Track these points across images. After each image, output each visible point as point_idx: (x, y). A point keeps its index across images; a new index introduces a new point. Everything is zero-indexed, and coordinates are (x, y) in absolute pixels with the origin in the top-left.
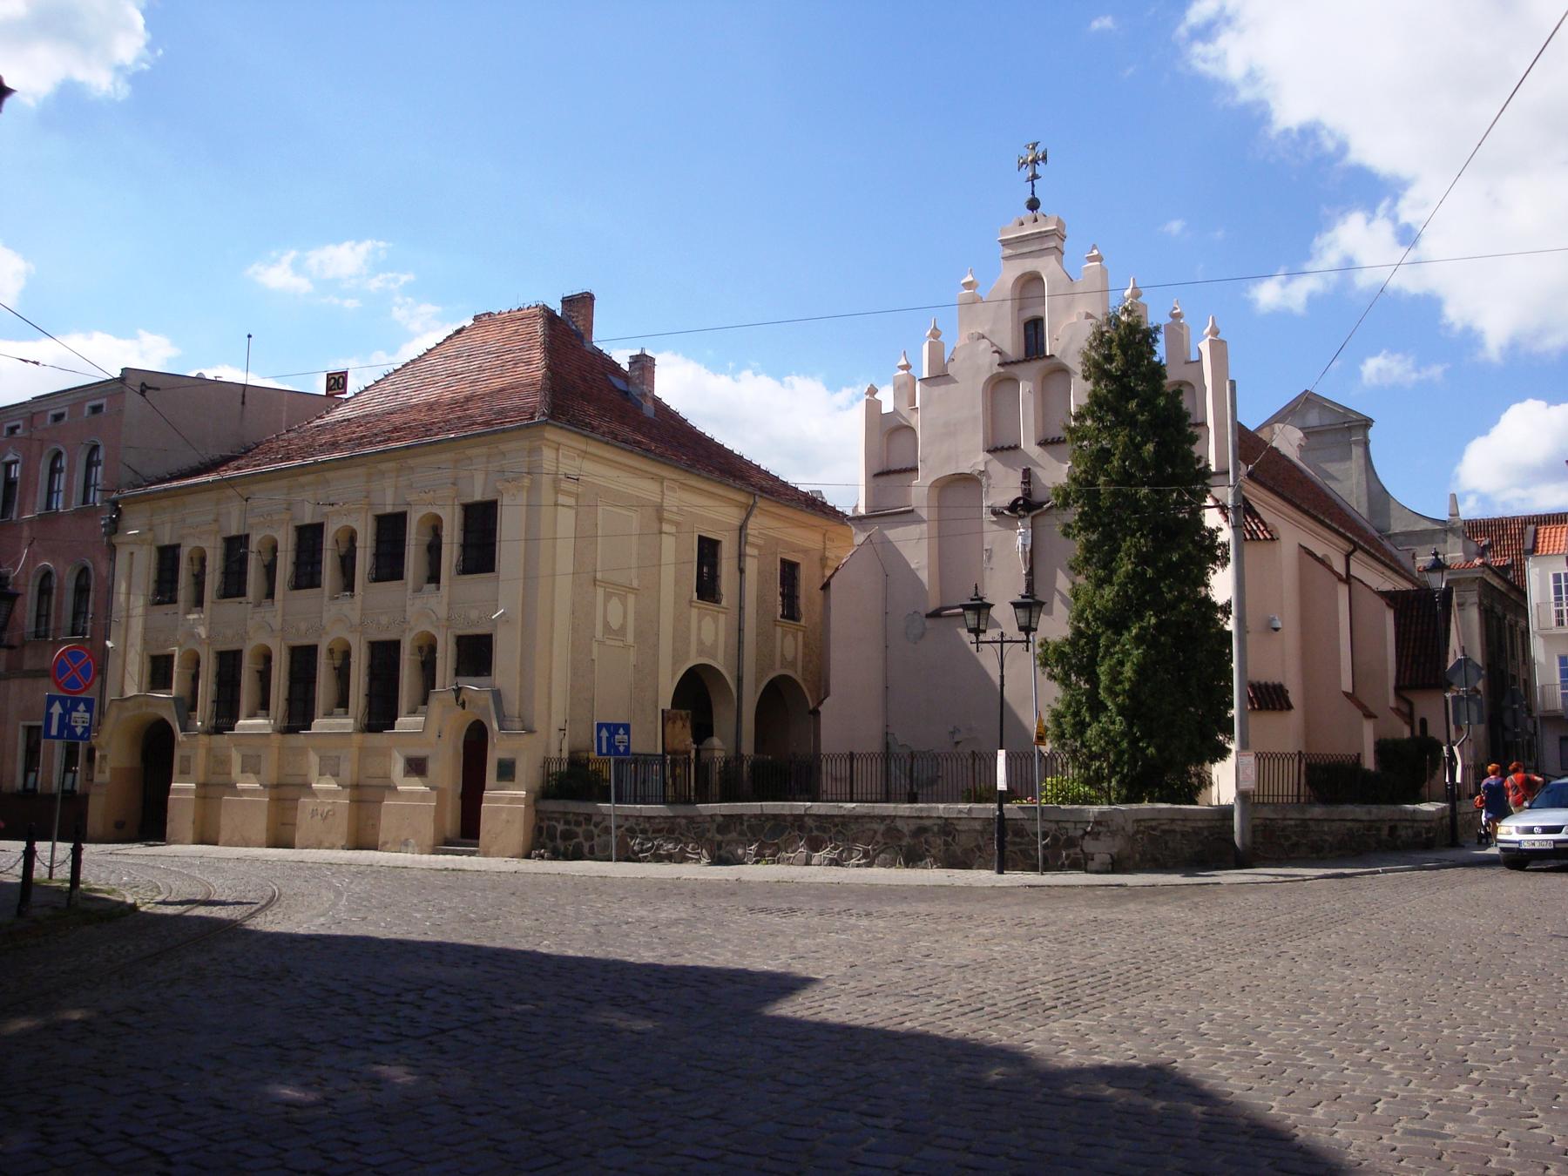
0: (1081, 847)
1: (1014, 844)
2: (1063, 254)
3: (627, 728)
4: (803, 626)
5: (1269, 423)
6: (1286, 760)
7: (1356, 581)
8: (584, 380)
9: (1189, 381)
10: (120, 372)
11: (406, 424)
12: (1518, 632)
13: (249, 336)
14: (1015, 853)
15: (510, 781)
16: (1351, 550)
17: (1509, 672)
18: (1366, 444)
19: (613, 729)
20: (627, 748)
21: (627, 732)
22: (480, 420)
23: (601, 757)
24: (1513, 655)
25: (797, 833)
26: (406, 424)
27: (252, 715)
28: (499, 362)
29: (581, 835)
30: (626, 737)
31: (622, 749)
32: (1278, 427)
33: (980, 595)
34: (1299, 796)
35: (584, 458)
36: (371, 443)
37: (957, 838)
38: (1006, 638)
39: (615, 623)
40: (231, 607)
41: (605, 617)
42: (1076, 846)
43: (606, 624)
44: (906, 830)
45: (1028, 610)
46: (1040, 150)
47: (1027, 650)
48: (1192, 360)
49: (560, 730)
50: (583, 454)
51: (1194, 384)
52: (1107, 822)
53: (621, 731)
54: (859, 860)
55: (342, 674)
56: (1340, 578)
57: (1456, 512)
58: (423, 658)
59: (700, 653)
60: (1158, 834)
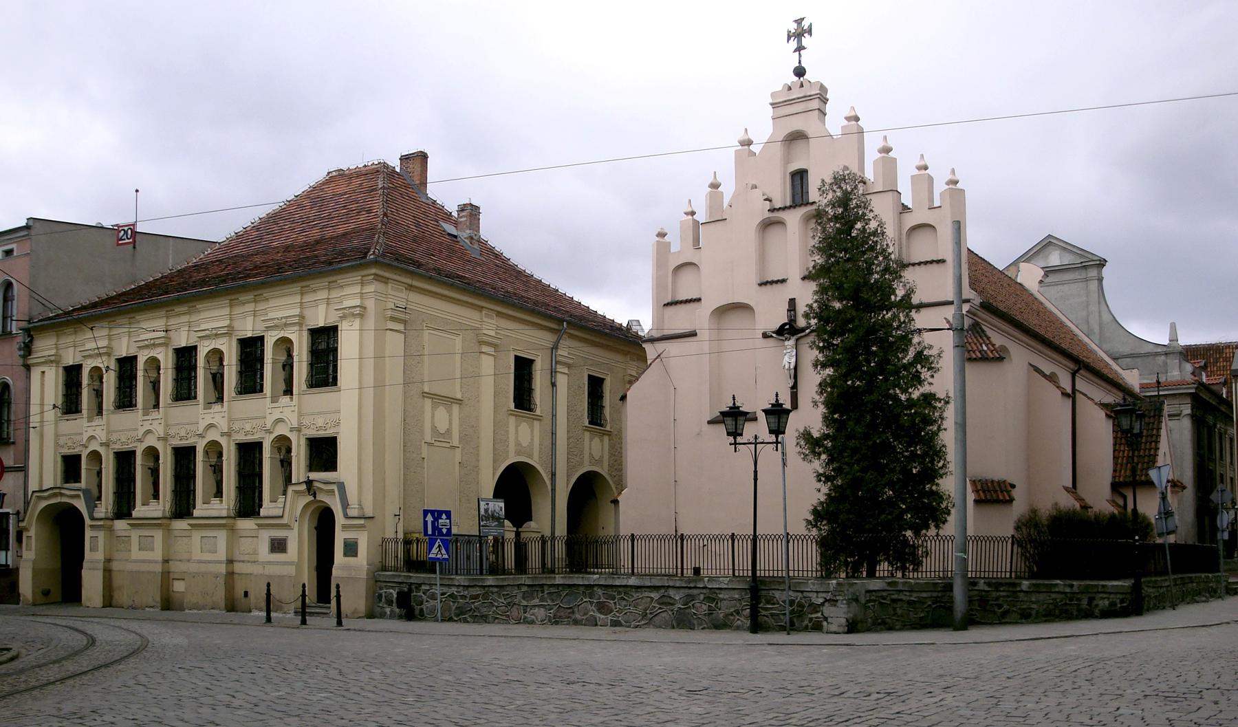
0: (822, 612)
1: (766, 609)
2: (825, 115)
3: (448, 514)
4: (608, 431)
5: (1015, 263)
6: (996, 543)
7: (1081, 395)
8: (418, 225)
9: (932, 224)
10: (26, 221)
11: (264, 263)
12: (1217, 434)
13: (137, 191)
14: (767, 616)
15: (353, 556)
16: (1076, 368)
17: (812, 354)
18: (1100, 280)
19: (437, 514)
20: (449, 530)
21: (449, 517)
22: (323, 259)
23: (427, 537)
24: (1221, 458)
26: (264, 263)
28: (345, 211)
30: (448, 521)
31: (444, 531)
32: (1023, 266)
33: (738, 404)
34: (1011, 572)
35: (410, 290)
36: (234, 279)
38: (759, 440)
39: (442, 428)
41: (516, 438)
42: (818, 612)
43: (434, 428)
45: (777, 416)
46: (805, 24)
47: (777, 450)
48: (935, 206)
50: (409, 288)
53: (444, 516)
54: (639, 622)
56: (1065, 394)
57: (1175, 338)
58: (282, 457)
59: (518, 453)
60: (888, 602)
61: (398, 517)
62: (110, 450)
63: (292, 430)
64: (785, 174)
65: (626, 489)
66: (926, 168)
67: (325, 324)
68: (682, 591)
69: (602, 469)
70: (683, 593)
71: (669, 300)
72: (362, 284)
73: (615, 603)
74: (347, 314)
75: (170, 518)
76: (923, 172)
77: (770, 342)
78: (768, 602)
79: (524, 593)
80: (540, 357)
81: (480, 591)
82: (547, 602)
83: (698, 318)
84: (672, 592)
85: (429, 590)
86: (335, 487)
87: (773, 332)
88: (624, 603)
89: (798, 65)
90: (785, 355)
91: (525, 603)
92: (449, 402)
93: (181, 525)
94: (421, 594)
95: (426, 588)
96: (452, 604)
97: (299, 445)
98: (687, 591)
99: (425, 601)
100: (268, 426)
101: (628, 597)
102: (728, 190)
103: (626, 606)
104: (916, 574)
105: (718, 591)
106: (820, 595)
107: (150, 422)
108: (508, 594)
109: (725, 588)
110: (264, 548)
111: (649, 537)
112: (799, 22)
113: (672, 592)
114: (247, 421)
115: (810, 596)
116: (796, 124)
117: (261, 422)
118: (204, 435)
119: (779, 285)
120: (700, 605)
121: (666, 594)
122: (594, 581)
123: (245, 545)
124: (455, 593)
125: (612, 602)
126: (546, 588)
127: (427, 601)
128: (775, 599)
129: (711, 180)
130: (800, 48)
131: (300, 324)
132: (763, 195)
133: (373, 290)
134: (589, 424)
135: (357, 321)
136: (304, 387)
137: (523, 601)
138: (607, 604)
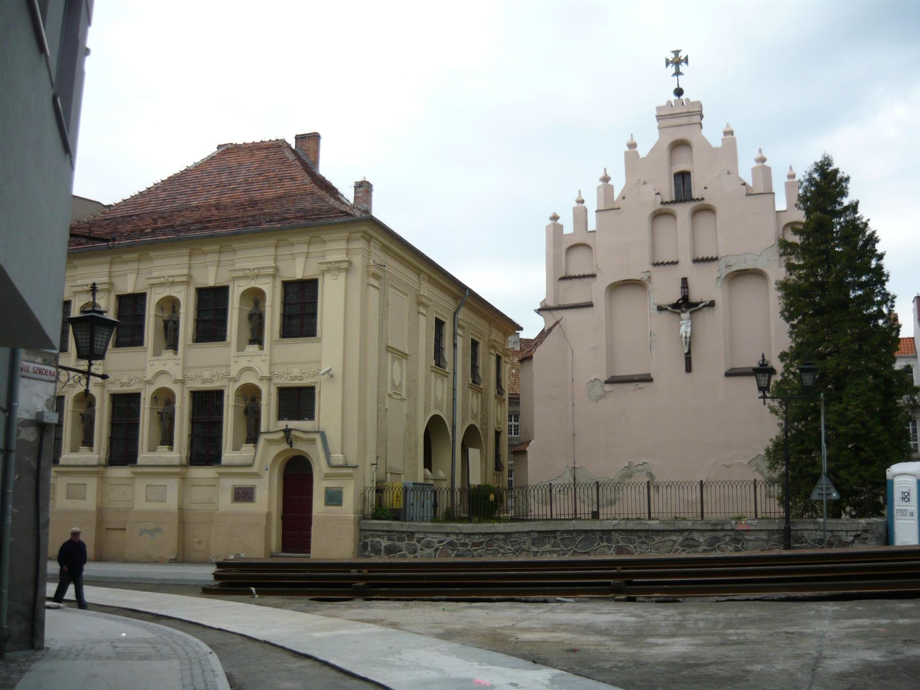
25: (605, 544)
27: (74, 450)
29: (404, 549)
37: (745, 545)
40: (210, 352)
41: (392, 375)
44: (702, 540)
49: (372, 464)
51: (591, 246)
52: (873, 530)
55: (166, 419)
61: (375, 466)
62: (186, 389)
63: (176, 382)
64: (670, 175)
65: (533, 441)
66: (583, 202)
67: (215, 284)
68: (706, 534)
69: (477, 422)
70: (708, 535)
71: (563, 275)
72: (348, 240)
73: (635, 547)
74: (333, 268)
75: (105, 466)
76: (580, 205)
77: (664, 314)
78: (797, 542)
79: (534, 539)
80: (448, 320)
81: (484, 538)
82: (560, 547)
83: (596, 291)
84: (696, 536)
85: (423, 538)
86: (317, 437)
87: (670, 305)
88: (644, 546)
89: (677, 87)
90: (682, 325)
91: (535, 549)
92: (401, 356)
93: (121, 472)
94: (415, 542)
95: (420, 536)
96: (450, 551)
97: (270, 394)
98: (711, 534)
99: (419, 548)
100: (234, 373)
101: (650, 541)
102: (619, 184)
103: (647, 549)
104: (609, 508)
105: (744, 533)
106: (850, 533)
107: (249, 358)
108: (515, 541)
109: (753, 530)
110: (225, 501)
111: (588, 485)
112: (677, 52)
113: (696, 536)
114: (205, 369)
115: (840, 535)
116: (681, 134)
117: (223, 371)
118: (152, 382)
119: (672, 266)
120: (725, 546)
121: (690, 537)
122: (614, 526)
123: (198, 496)
124: (454, 540)
125: (631, 546)
126: (558, 534)
127: (421, 550)
128: (803, 539)
129: (602, 174)
130: (678, 73)
131: (274, 276)
132: (655, 190)
133: (361, 247)
134: (472, 382)
135: (342, 276)
136: (190, 342)
137: (532, 547)
138: (627, 547)
